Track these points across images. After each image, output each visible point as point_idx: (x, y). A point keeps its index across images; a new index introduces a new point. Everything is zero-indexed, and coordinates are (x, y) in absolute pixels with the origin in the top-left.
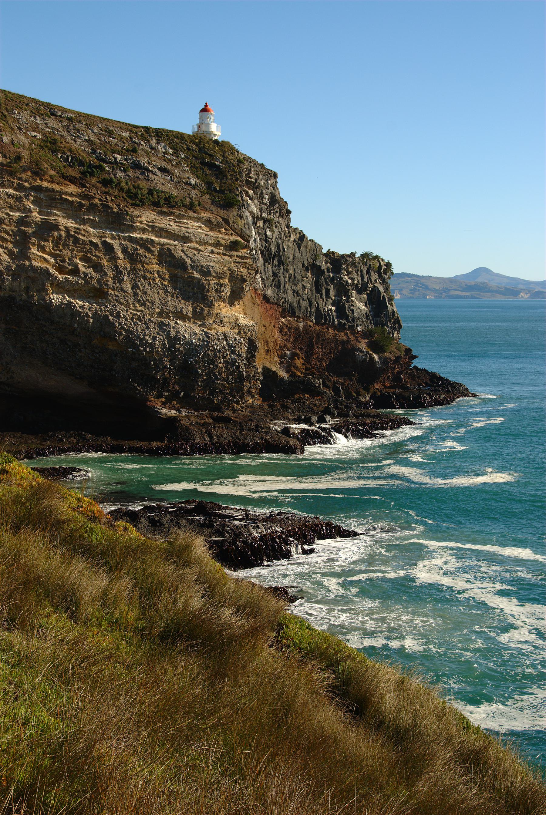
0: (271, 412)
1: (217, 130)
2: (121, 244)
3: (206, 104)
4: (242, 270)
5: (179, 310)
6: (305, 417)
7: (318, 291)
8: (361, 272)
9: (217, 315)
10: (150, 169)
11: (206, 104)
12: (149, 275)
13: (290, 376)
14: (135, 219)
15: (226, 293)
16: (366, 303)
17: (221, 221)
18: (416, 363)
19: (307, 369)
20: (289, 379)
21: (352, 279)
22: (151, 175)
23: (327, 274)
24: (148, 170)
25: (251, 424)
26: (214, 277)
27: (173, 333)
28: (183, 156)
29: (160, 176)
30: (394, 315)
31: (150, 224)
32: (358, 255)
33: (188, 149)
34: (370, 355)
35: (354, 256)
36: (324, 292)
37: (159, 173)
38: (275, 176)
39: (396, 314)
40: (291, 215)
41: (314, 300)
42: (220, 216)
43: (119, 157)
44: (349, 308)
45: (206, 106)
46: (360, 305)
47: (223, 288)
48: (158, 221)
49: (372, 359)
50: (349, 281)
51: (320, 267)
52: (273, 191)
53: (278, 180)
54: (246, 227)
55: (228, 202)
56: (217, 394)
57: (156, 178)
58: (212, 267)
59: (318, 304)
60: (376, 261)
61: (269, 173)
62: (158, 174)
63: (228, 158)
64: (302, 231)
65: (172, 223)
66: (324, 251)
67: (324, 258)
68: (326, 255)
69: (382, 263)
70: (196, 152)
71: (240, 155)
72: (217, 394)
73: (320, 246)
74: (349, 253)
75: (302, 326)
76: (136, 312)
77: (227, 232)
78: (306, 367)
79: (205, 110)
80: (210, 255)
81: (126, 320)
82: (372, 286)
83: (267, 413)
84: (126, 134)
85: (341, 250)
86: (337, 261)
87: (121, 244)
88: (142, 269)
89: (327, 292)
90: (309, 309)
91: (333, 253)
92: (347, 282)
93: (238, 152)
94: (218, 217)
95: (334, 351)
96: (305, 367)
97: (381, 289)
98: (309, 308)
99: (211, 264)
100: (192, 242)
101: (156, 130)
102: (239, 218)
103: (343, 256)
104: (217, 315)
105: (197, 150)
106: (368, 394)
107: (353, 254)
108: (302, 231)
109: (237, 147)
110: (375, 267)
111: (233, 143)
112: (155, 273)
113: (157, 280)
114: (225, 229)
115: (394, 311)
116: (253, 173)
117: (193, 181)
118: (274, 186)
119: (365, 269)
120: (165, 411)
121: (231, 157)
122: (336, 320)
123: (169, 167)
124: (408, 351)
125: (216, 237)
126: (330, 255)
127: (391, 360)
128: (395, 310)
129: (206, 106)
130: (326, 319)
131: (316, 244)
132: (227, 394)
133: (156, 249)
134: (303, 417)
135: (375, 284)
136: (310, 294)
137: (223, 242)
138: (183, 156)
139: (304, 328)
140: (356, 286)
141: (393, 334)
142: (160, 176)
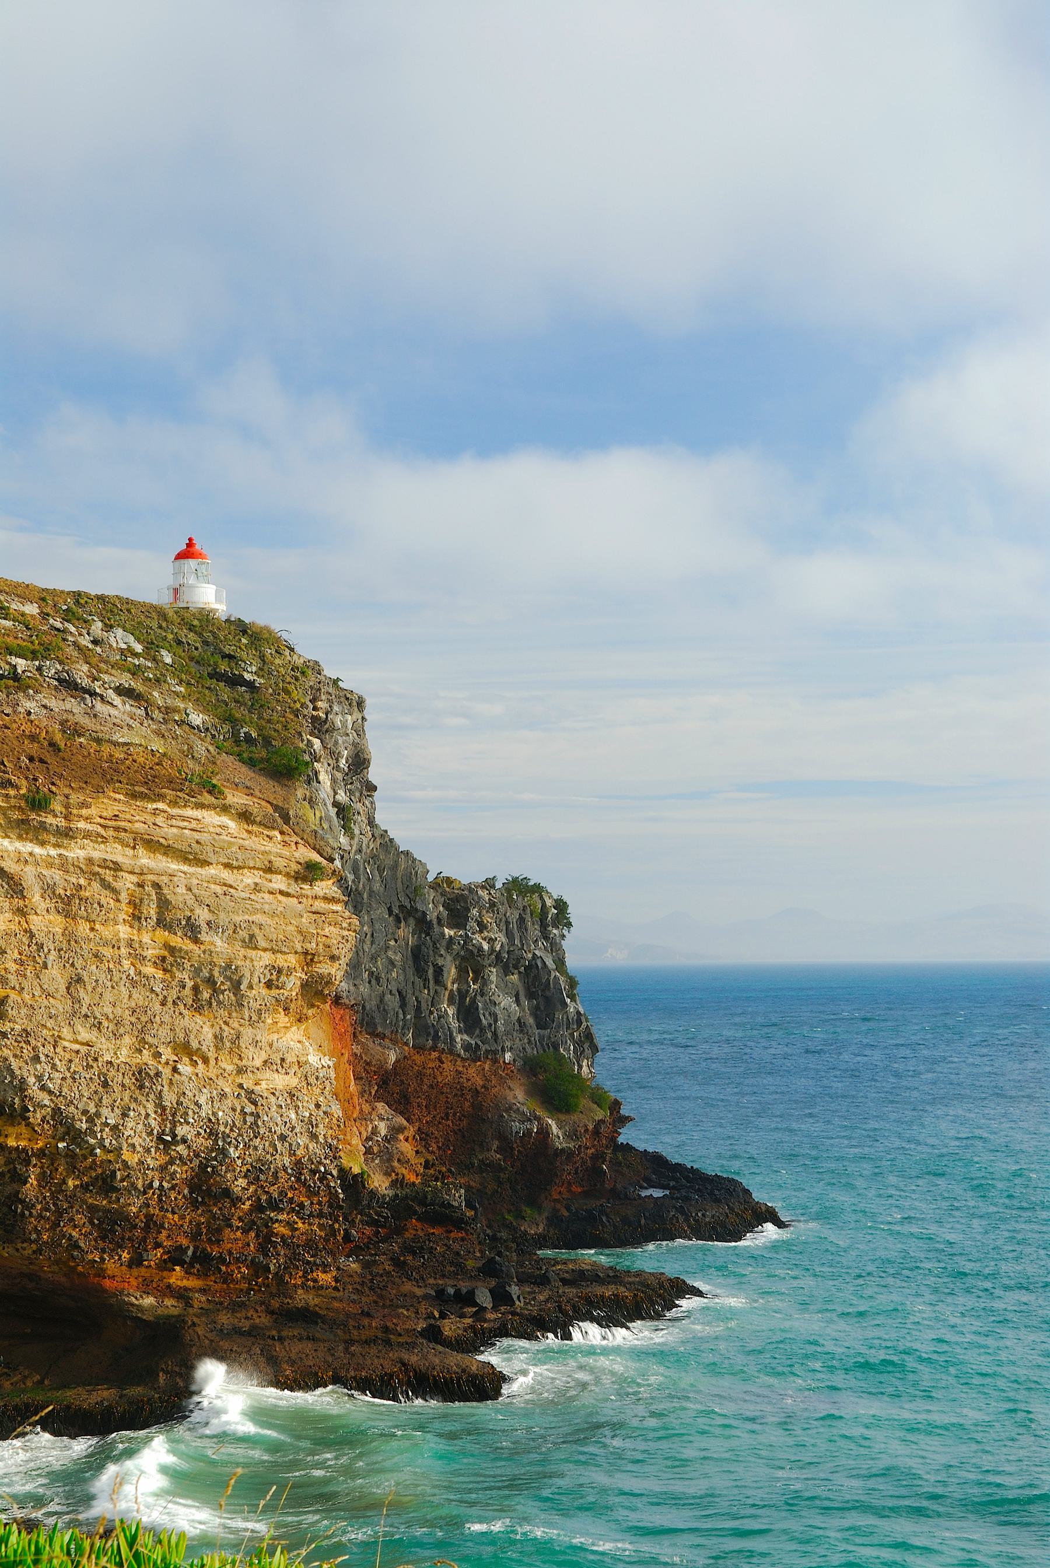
0: (372, 1281)
1: (218, 599)
2: (40, 876)
3: (190, 539)
4: (326, 932)
5: (182, 1036)
6: (458, 1292)
7: (420, 972)
8: (507, 923)
9: (271, 1046)
10: (98, 690)
12: (107, 952)
13: (394, 1184)
14: (75, 811)
15: (291, 990)
16: (517, 996)
17: (272, 811)
18: (626, 1136)
19: (427, 1165)
20: (391, 1193)
21: (491, 941)
22: (99, 706)
23: (436, 928)
24: (93, 694)
25: (370, 1325)
26: (265, 950)
27: (169, 1099)
28: (168, 660)
29: (120, 706)
30: (579, 1023)
31: (110, 823)
33: (179, 643)
34: (538, 1119)
35: (493, 886)
36: (431, 971)
37: (117, 701)
38: (360, 704)
39: (583, 1019)
41: (410, 992)
42: (268, 802)
43: (21, 664)
44: (485, 1009)
45: (190, 544)
46: (505, 1002)
47: (283, 978)
48: (128, 817)
49: (544, 1132)
50: (486, 946)
51: (424, 914)
52: (358, 740)
53: (366, 713)
54: (326, 826)
55: (285, 769)
56: (275, 1248)
57: (113, 712)
58: (260, 926)
59: (419, 1002)
60: (536, 896)
61: (347, 699)
62: (115, 703)
63: (272, 663)
64: (386, 831)
65: (160, 820)
66: (430, 878)
67: (432, 893)
68: (436, 885)
69: (549, 903)
70: (196, 649)
71: (295, 657)
72: (275, 1248)
73: (423, 865)
74: (480, 879)
75: (392, 1057)
76: (77, 1047)
77: (287, 838)
78: (427, 1162)
79: (188, 552)
80: (253, 897)
81: (54, 1067)
82: (530, 956)
83: (363, 1284)
84: (31, 609)
85: (467, 872)
86: (459, 903)
87: (40, 876)
88: (92, 935)
89: (439, 971)
90: (401, 1016)
91: (449, 881)
92: (480, 949)
93: (292, 650)
94: (264, 803)
95: (454, 1114)
96: (422, 1161)
97: (550, 963)
98: (401, 1011)
99: (259, 918)
100: (209, 864)
101: (101, 598)
102: (306, 803)
103: (470, 889)
104: (271, 1046)
105: (198, 645)
106: (540, 1214)
107: (489, 884)
108: (386, 831)
109: (285, 636)
110: (533, 911)
111: (276, 627)
112: (122, 944)
113: (126, 964)
114: (282, 833)
115: (578, 1013)
116: (323, 697)
117: (197, 719)
118: (360, 732)
119: (514, 916)
120: (149, 1301)
121: (277, 661)
122: (458, 1039)
123: (138, 686)
125: (264, 853)
126: (443, 883)
127: (586, 1130)
128: (582, 1011)
129: (190, 544)
130: (436, 1037)
131: (414, 860)
132: (298, 1246)
133: (127, 883)
134: (451, 1291)
135: (537, 952)
136: (401, 978)
137: (279, 863)
138: (168, 660)
139: (397, 1061)
140: (498, 956)
141: (580, 1067)
142: (120, 706)
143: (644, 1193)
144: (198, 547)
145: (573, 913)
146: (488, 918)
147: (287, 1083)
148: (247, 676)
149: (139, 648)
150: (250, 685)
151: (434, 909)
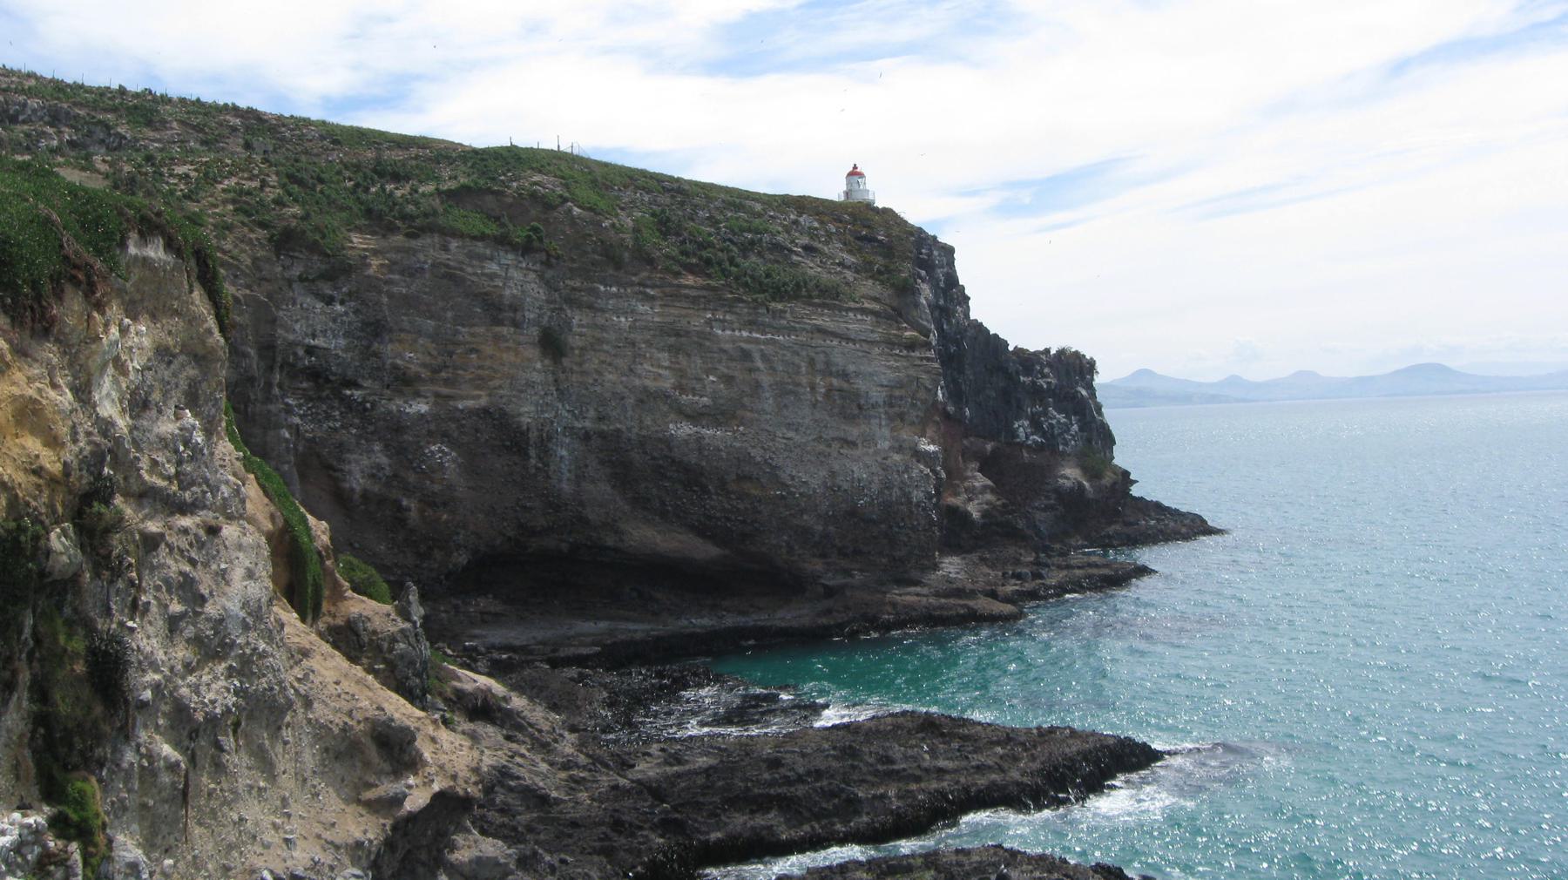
18: (1135, 491)
32: (1053, 352)
40: (971, 303)
45: (855, 167)
66: (1011, 348)
75: (989, 447)
84: (758, 207)
91: (1022, 350)
103: (1036, 354)
107: (1047, 351)
124: (1126, 474)
129: (855, 167)
143: (932, 448)
145: (1098, 366)
146: (1046, 370)
147: (893, 457)
149: (816, 225)
151: (1012, 368)
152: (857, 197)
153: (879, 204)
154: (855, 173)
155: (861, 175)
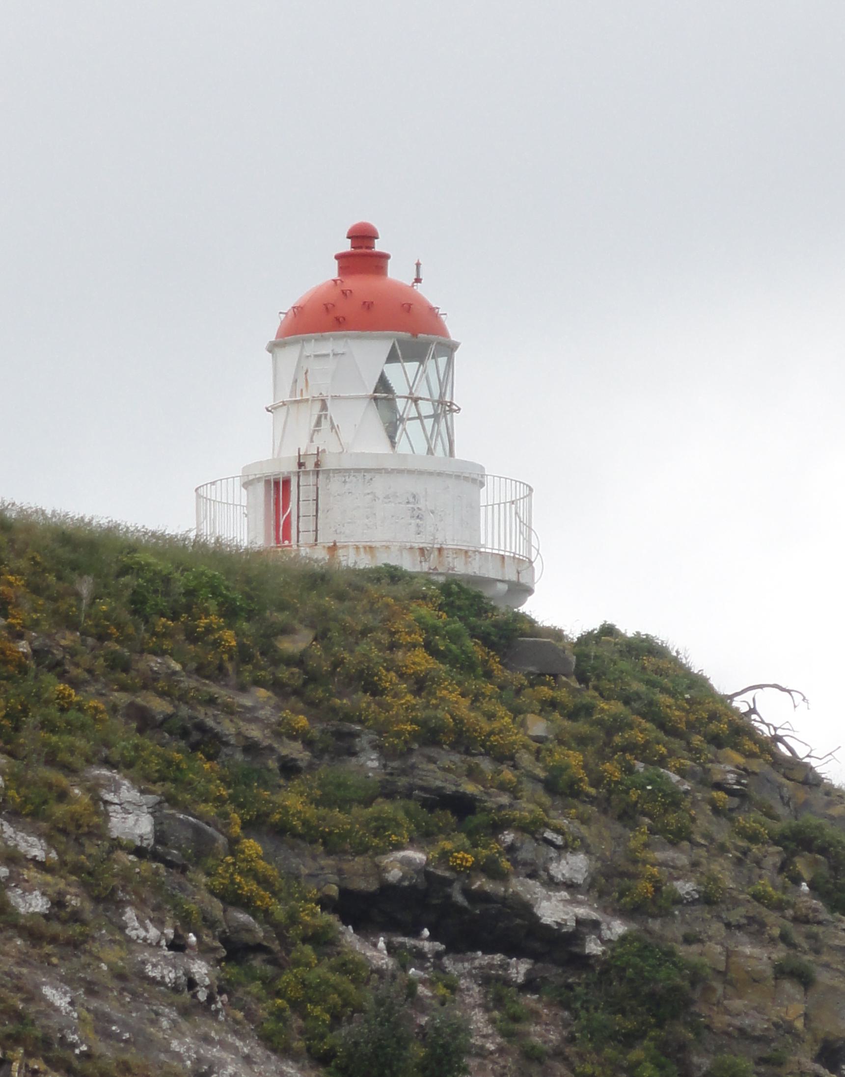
3: (363, 236)
11: (363, 236)
45: (362, 254)
129: (362, 254)
144: (398, 272)
148: (552, 910)
150: (557, 947)
152: (360, 531)
153: (562, 606)
154: (365, 302)
155: (415, 330)
